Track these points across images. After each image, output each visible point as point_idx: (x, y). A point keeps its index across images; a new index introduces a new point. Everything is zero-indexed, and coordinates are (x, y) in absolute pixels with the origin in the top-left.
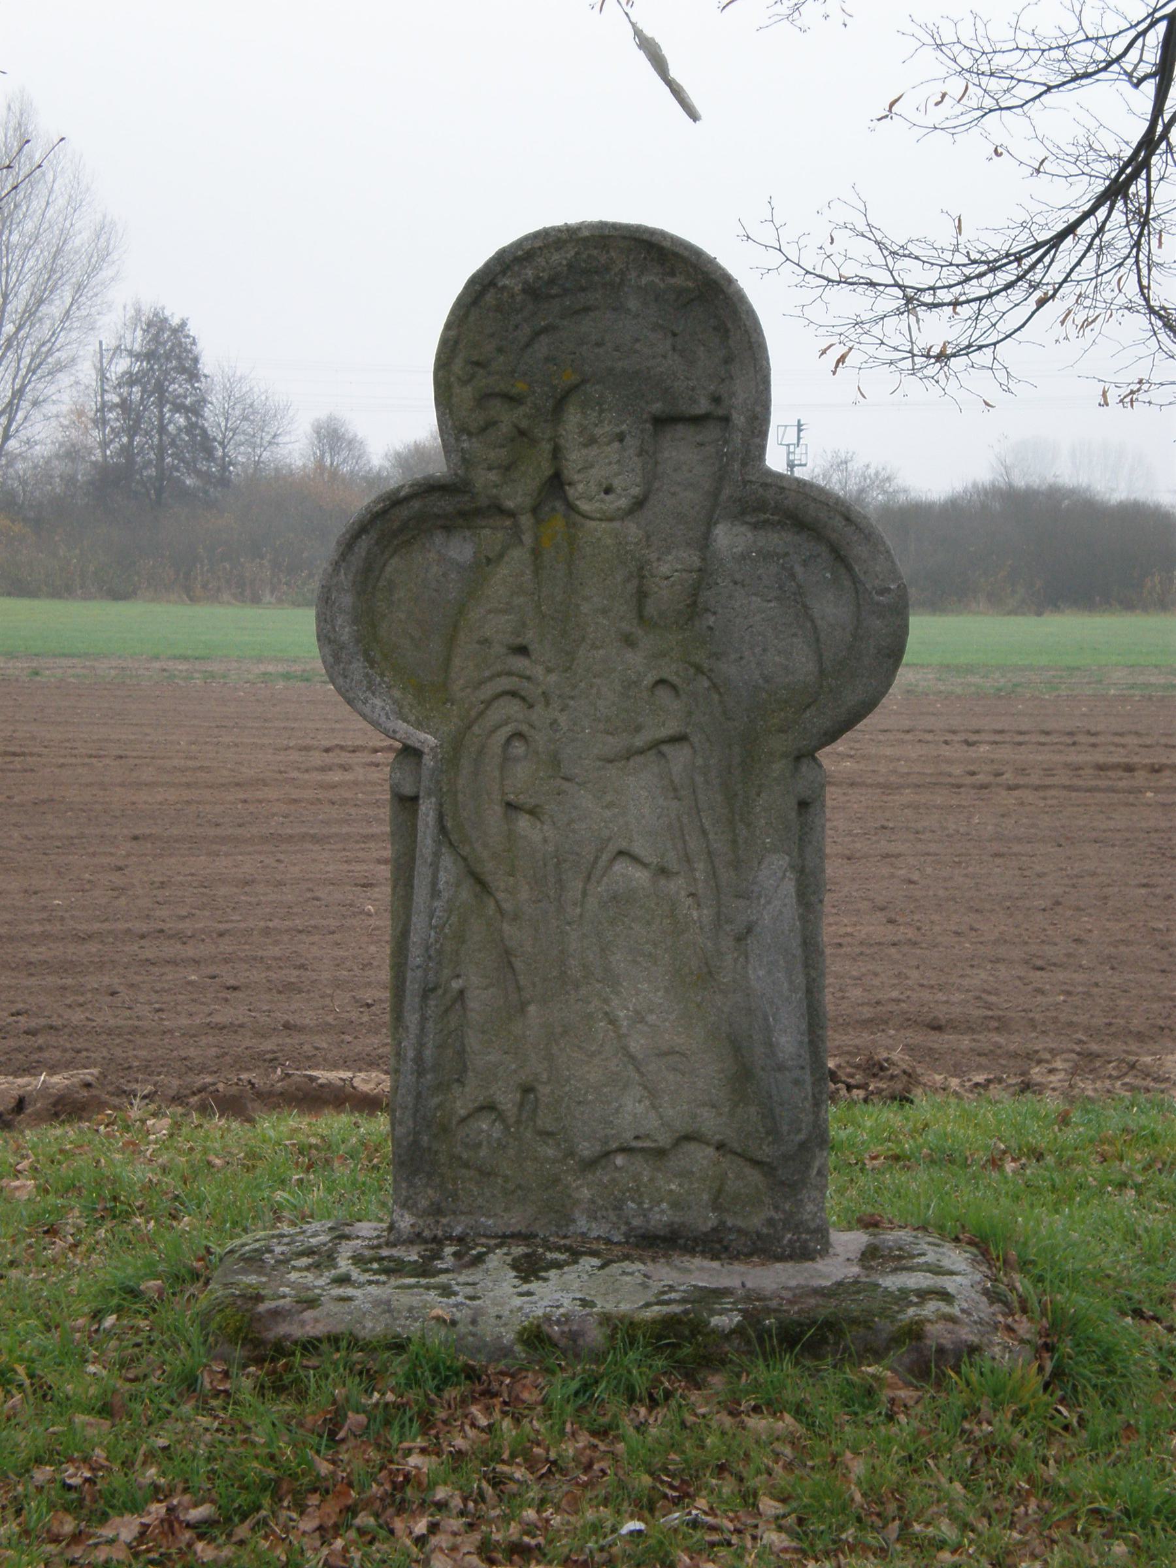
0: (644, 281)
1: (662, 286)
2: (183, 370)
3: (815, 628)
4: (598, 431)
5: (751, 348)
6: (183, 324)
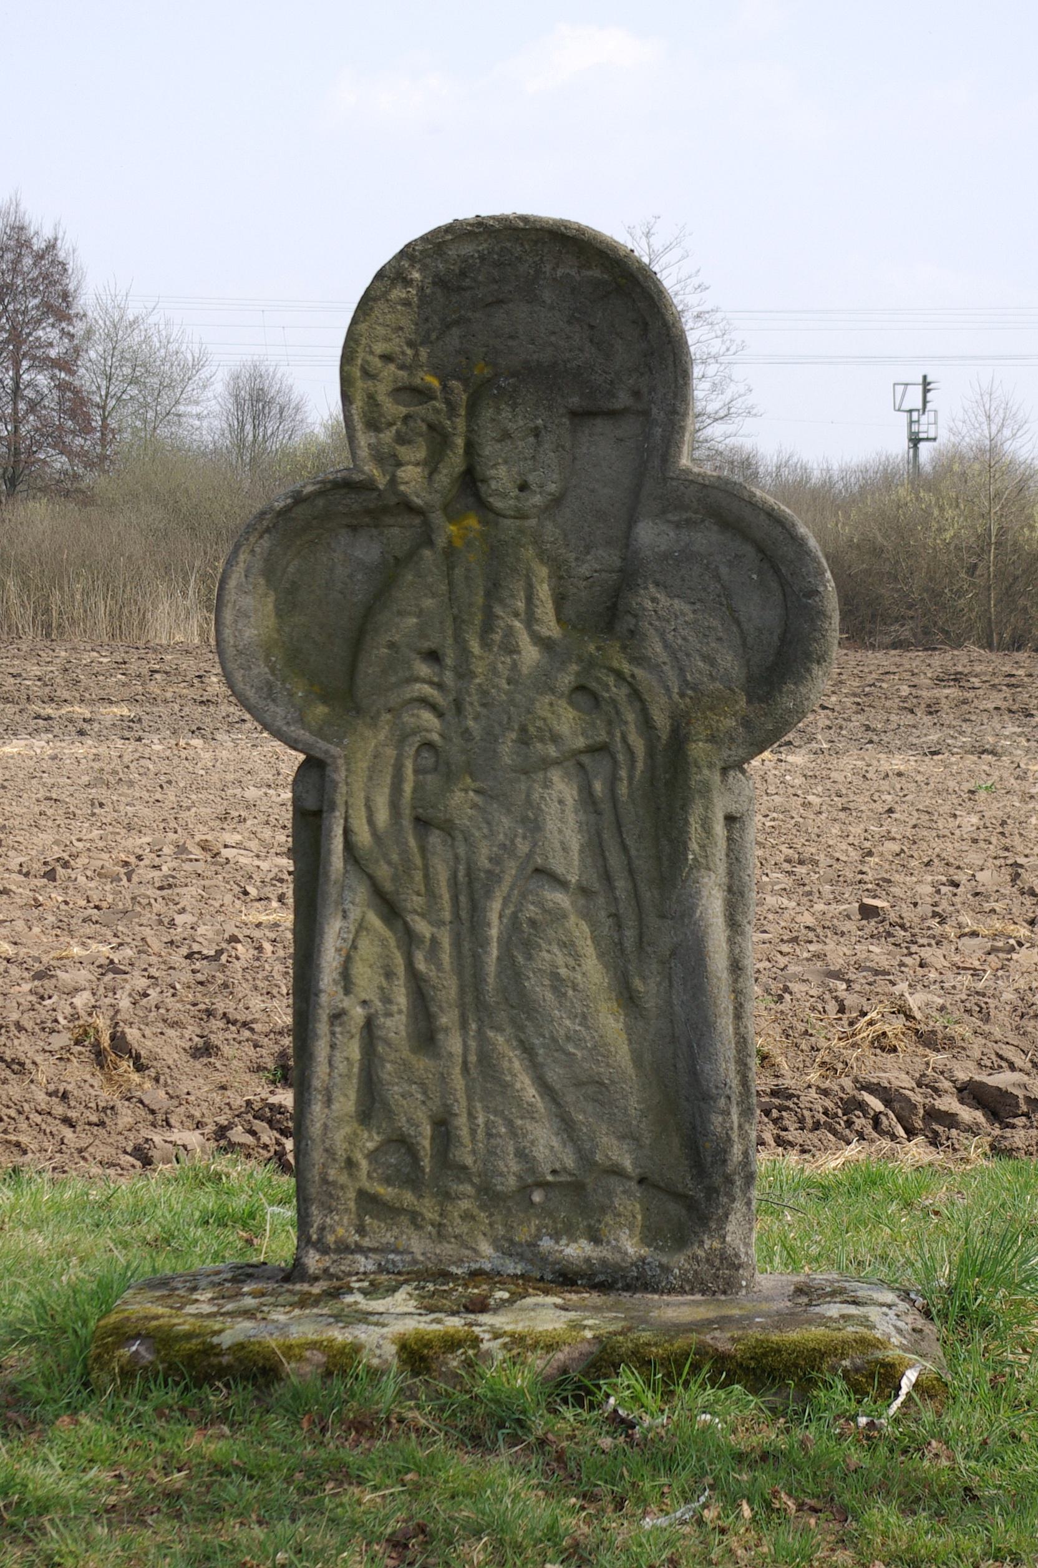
0: (559, 272)
1: (578, 278)
2: (48, 308)
3: (742, 631)
4: (511, 426)
5: (669, 342)
6: (51, 246)
